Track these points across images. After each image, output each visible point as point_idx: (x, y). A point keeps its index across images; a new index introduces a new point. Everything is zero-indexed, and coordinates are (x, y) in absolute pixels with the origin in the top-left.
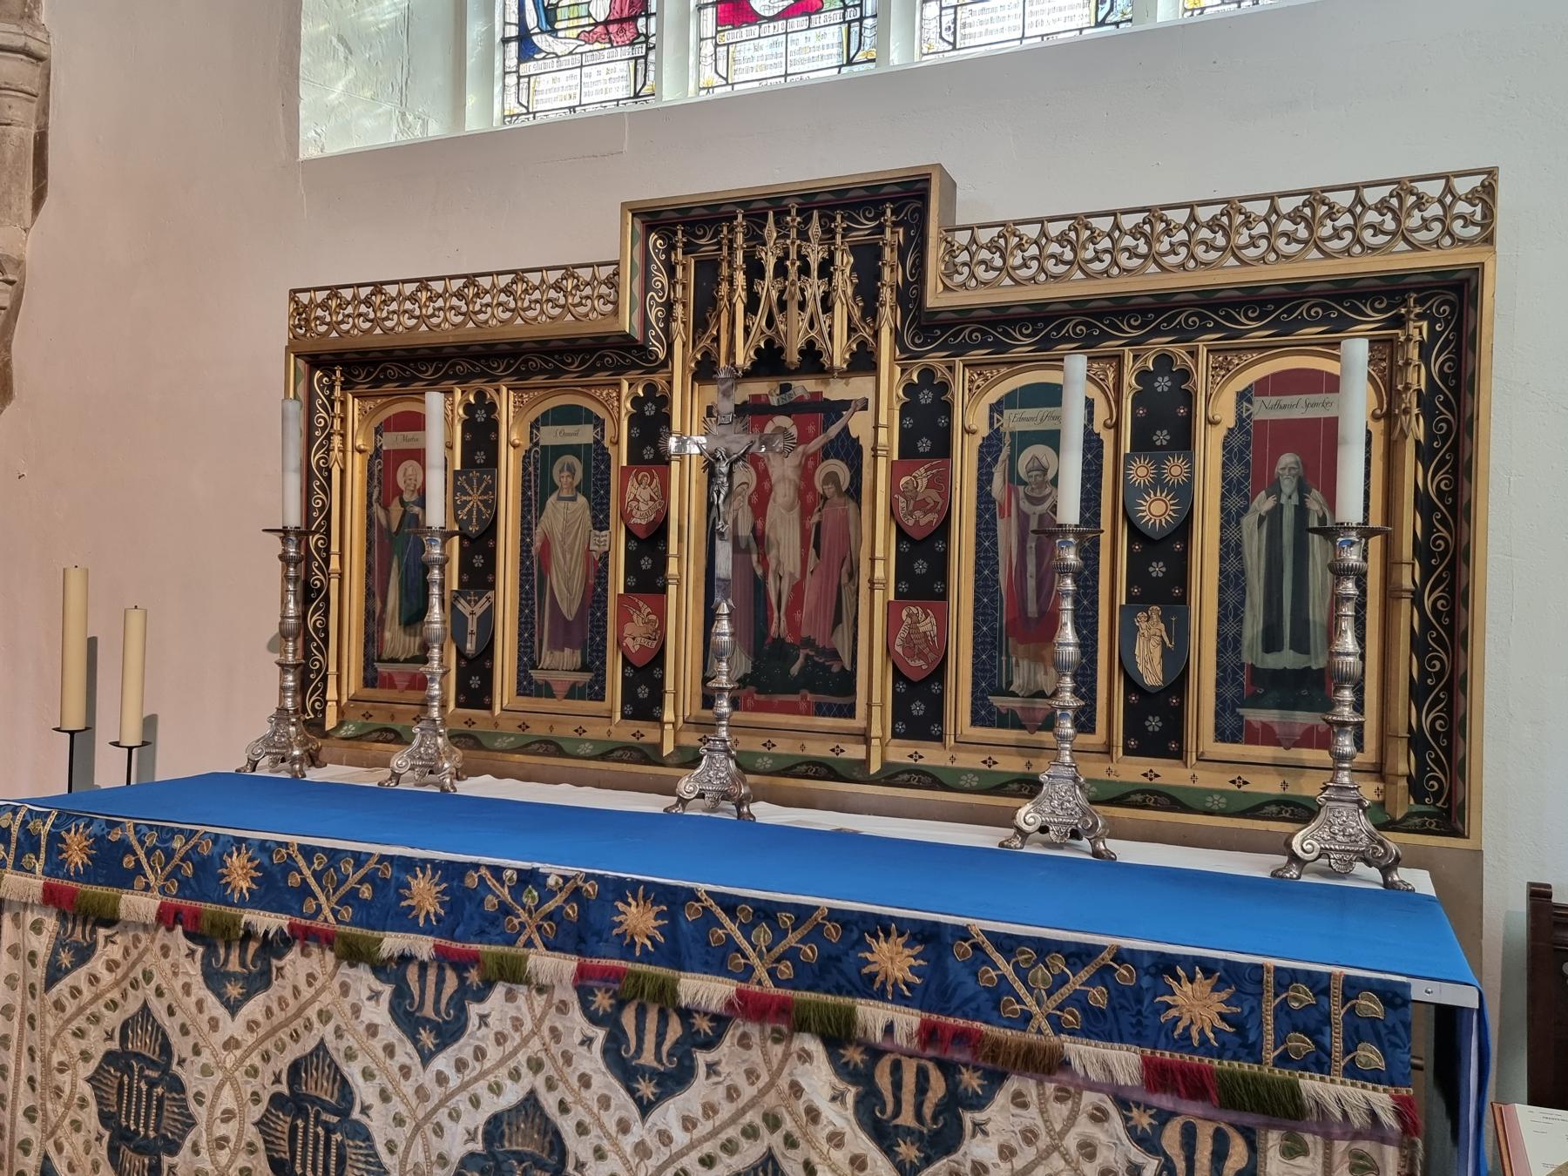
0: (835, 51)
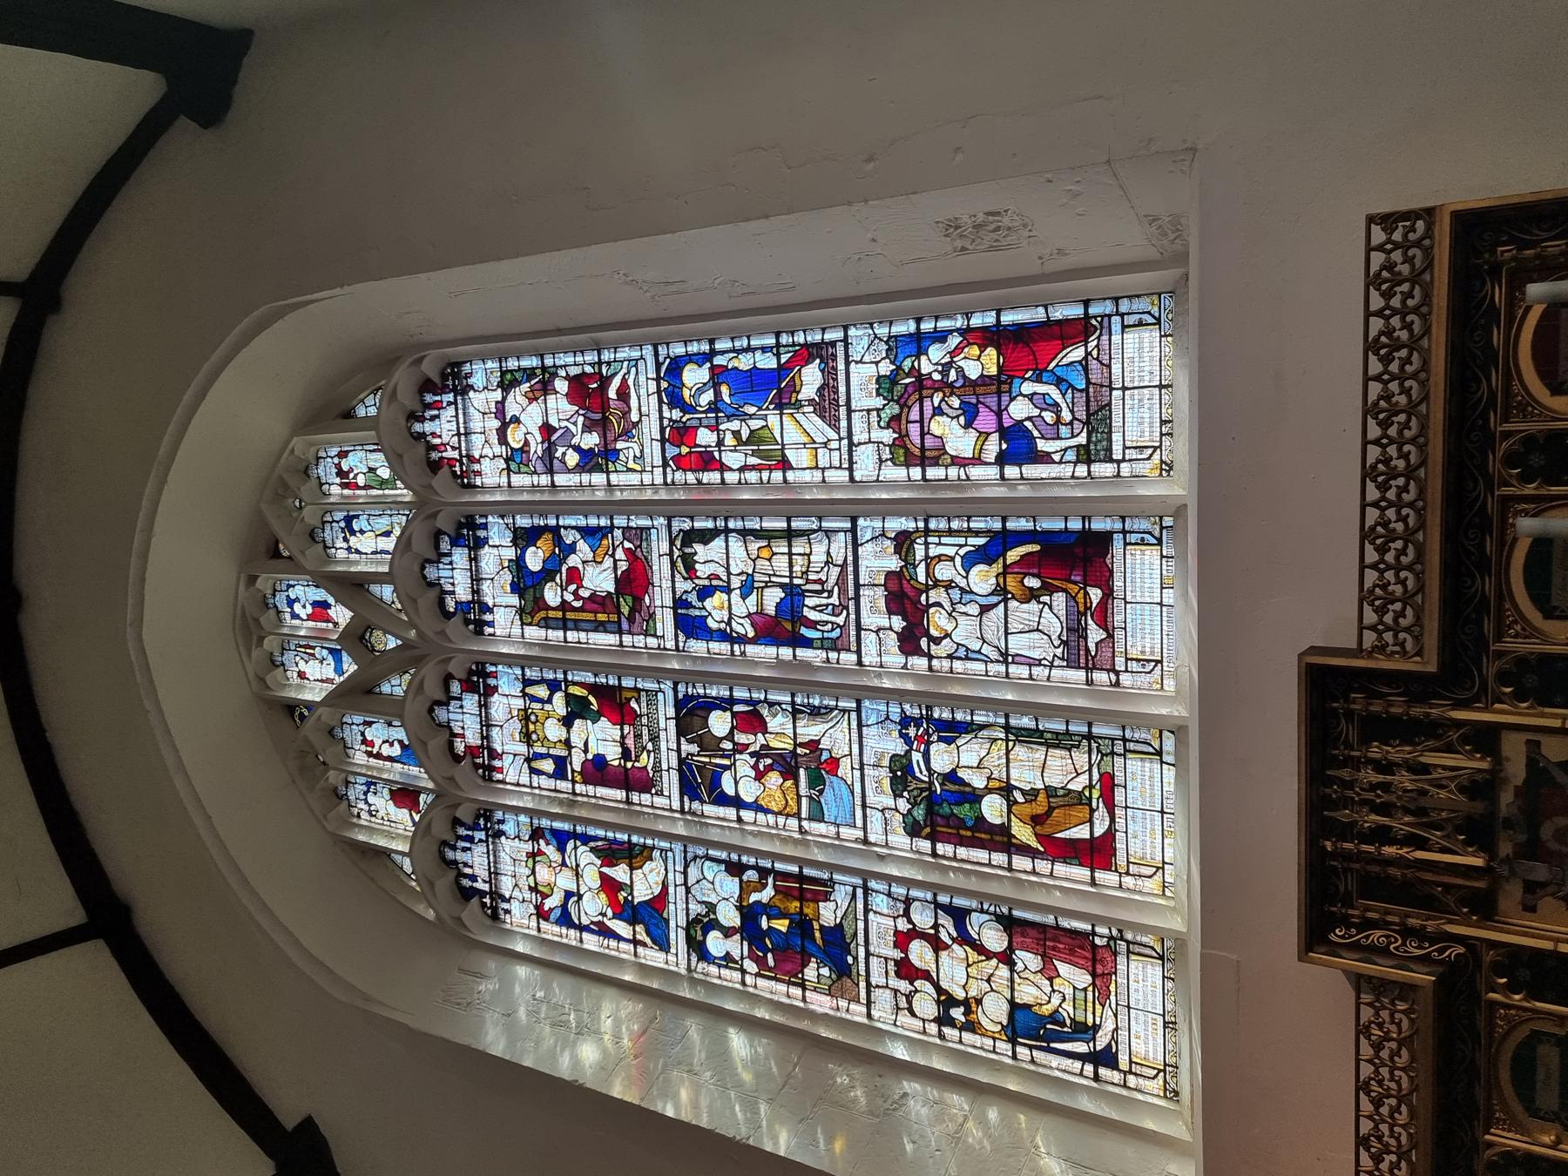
0: (1147, 765)
